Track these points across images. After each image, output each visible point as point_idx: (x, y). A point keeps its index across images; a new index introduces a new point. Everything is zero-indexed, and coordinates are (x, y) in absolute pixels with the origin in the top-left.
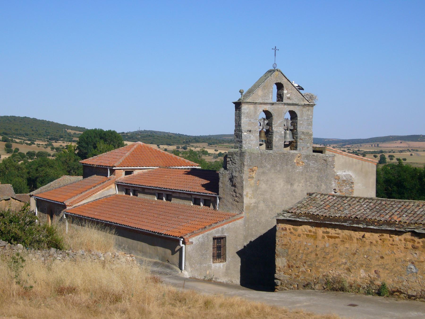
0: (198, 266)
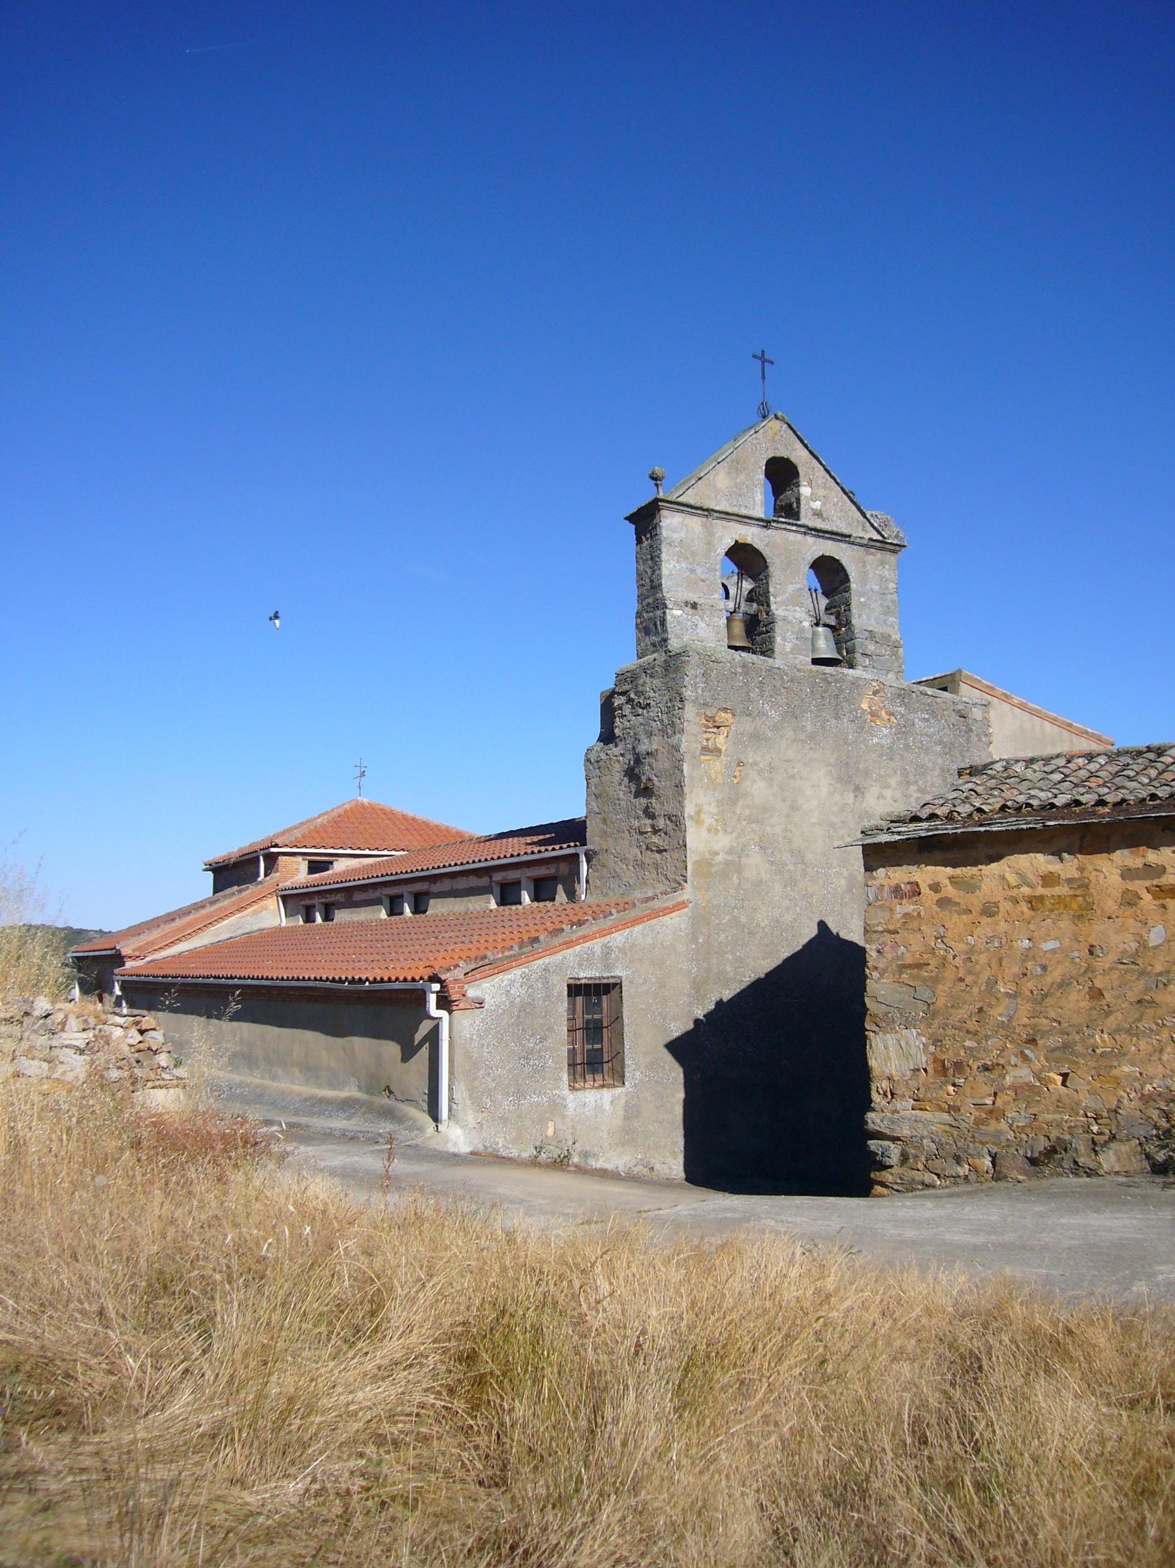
0: (507, 1104)
